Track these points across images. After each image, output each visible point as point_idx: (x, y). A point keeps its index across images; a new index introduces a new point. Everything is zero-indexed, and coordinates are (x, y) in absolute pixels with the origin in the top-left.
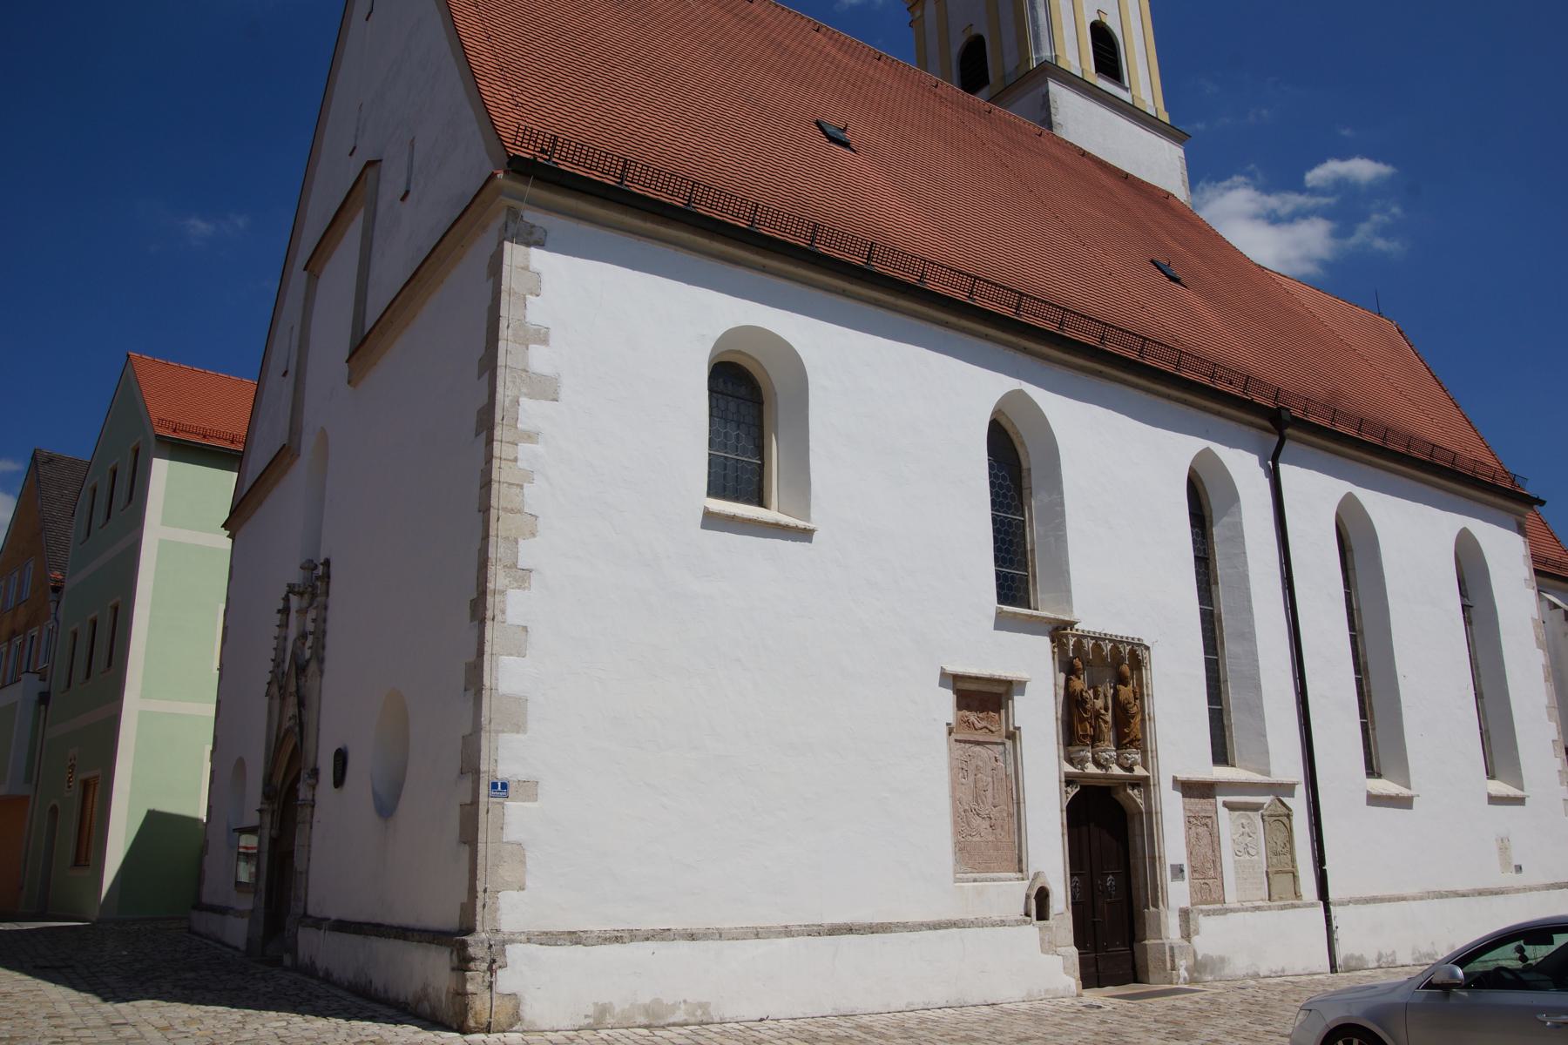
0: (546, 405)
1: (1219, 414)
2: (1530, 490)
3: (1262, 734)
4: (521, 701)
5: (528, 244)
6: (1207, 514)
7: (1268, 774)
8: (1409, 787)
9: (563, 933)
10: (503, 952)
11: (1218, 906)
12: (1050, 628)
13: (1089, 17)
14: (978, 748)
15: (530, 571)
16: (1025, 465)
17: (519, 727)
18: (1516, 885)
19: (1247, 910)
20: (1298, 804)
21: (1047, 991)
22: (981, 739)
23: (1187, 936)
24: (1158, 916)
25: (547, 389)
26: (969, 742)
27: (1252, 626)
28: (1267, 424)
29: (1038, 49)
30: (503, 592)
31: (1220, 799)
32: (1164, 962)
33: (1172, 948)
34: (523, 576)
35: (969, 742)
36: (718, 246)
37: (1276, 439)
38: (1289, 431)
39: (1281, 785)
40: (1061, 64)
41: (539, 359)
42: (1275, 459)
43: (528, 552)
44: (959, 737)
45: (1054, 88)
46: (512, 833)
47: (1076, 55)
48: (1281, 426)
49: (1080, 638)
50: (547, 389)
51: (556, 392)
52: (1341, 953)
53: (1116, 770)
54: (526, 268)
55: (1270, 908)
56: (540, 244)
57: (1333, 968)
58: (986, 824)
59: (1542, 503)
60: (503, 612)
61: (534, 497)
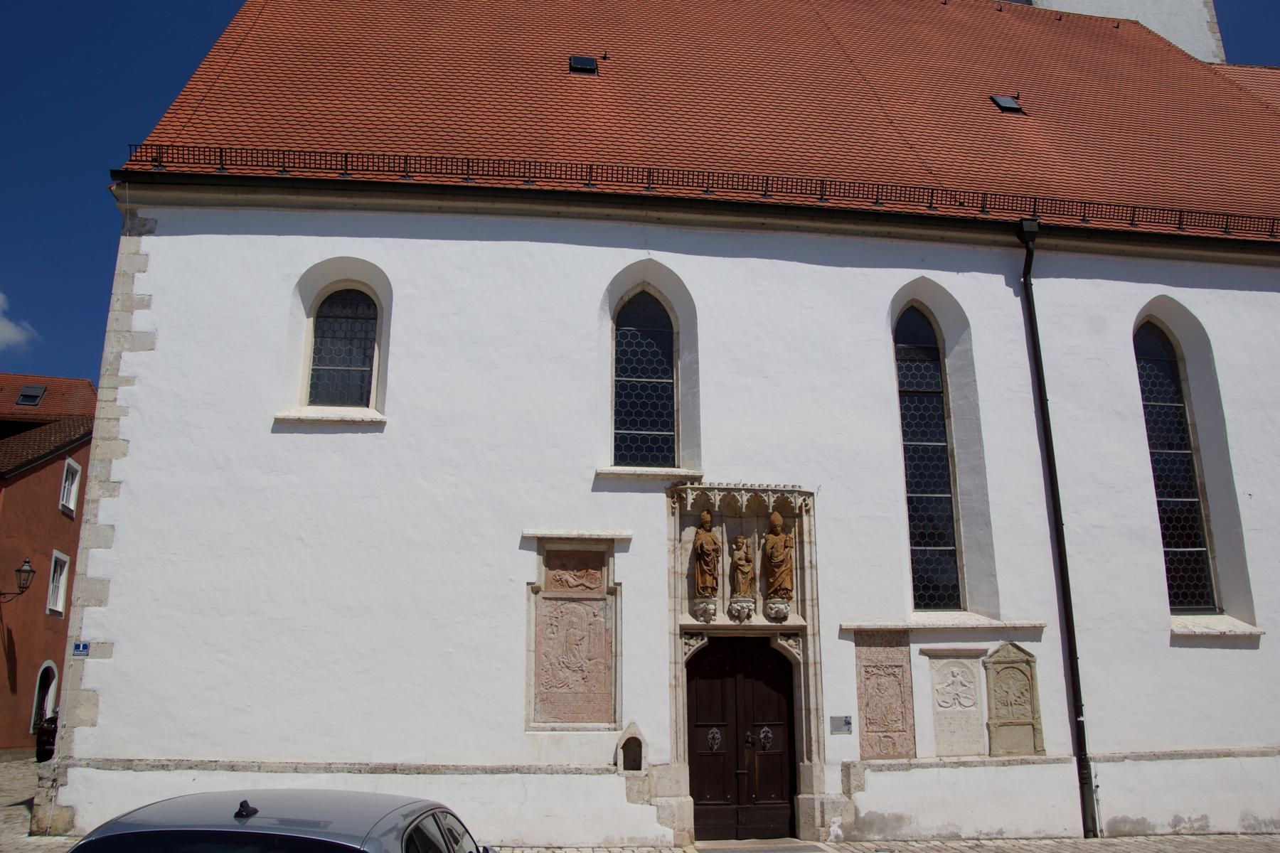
0: (143, 355)
4: (104, 583)
5: (140, 235)
6: (940, 346)
7: (997, 617)
8: (1254, 624)
9: (120, 760)
10: (66, 773)
11: (905, 761)
12: (668, 485)
14: (574, 605)
15: (120, 483)
16: (675, 330)
17: (101, 602)
19: (944, 766)
20: (1048, 653)
21: (631, 839)
22: (575, 596)
23: (847, 792)
24: (816, 771)
25: (146, 342)
26: (562, 599)
27: (982, 458)
28: (1015, 239)
30: (96, 501)
31: (915, 648)
32: (813, 818)
33: (822, 804)
34: (113, 487)
35: (562, 599)
36: (305, 199)
37: (1023, 252)
38: (1038, 241)
39: (1015, 628)
41: (141, 321)
42: (1027, 273)
43: (119, 469)
44: (548, 595)
46: (88, 683)
48: (1027, 238)
49: (704, 492)
50: (146, 342)
51: (153, 343)
52: (1104, 816)
53: (758, 620)
54: (137, 253)
55: (991, 764)
56: (150, 232)
57: (1090, 829)
58: (579, 676)
60: (96, 516)
61: (126, 427)
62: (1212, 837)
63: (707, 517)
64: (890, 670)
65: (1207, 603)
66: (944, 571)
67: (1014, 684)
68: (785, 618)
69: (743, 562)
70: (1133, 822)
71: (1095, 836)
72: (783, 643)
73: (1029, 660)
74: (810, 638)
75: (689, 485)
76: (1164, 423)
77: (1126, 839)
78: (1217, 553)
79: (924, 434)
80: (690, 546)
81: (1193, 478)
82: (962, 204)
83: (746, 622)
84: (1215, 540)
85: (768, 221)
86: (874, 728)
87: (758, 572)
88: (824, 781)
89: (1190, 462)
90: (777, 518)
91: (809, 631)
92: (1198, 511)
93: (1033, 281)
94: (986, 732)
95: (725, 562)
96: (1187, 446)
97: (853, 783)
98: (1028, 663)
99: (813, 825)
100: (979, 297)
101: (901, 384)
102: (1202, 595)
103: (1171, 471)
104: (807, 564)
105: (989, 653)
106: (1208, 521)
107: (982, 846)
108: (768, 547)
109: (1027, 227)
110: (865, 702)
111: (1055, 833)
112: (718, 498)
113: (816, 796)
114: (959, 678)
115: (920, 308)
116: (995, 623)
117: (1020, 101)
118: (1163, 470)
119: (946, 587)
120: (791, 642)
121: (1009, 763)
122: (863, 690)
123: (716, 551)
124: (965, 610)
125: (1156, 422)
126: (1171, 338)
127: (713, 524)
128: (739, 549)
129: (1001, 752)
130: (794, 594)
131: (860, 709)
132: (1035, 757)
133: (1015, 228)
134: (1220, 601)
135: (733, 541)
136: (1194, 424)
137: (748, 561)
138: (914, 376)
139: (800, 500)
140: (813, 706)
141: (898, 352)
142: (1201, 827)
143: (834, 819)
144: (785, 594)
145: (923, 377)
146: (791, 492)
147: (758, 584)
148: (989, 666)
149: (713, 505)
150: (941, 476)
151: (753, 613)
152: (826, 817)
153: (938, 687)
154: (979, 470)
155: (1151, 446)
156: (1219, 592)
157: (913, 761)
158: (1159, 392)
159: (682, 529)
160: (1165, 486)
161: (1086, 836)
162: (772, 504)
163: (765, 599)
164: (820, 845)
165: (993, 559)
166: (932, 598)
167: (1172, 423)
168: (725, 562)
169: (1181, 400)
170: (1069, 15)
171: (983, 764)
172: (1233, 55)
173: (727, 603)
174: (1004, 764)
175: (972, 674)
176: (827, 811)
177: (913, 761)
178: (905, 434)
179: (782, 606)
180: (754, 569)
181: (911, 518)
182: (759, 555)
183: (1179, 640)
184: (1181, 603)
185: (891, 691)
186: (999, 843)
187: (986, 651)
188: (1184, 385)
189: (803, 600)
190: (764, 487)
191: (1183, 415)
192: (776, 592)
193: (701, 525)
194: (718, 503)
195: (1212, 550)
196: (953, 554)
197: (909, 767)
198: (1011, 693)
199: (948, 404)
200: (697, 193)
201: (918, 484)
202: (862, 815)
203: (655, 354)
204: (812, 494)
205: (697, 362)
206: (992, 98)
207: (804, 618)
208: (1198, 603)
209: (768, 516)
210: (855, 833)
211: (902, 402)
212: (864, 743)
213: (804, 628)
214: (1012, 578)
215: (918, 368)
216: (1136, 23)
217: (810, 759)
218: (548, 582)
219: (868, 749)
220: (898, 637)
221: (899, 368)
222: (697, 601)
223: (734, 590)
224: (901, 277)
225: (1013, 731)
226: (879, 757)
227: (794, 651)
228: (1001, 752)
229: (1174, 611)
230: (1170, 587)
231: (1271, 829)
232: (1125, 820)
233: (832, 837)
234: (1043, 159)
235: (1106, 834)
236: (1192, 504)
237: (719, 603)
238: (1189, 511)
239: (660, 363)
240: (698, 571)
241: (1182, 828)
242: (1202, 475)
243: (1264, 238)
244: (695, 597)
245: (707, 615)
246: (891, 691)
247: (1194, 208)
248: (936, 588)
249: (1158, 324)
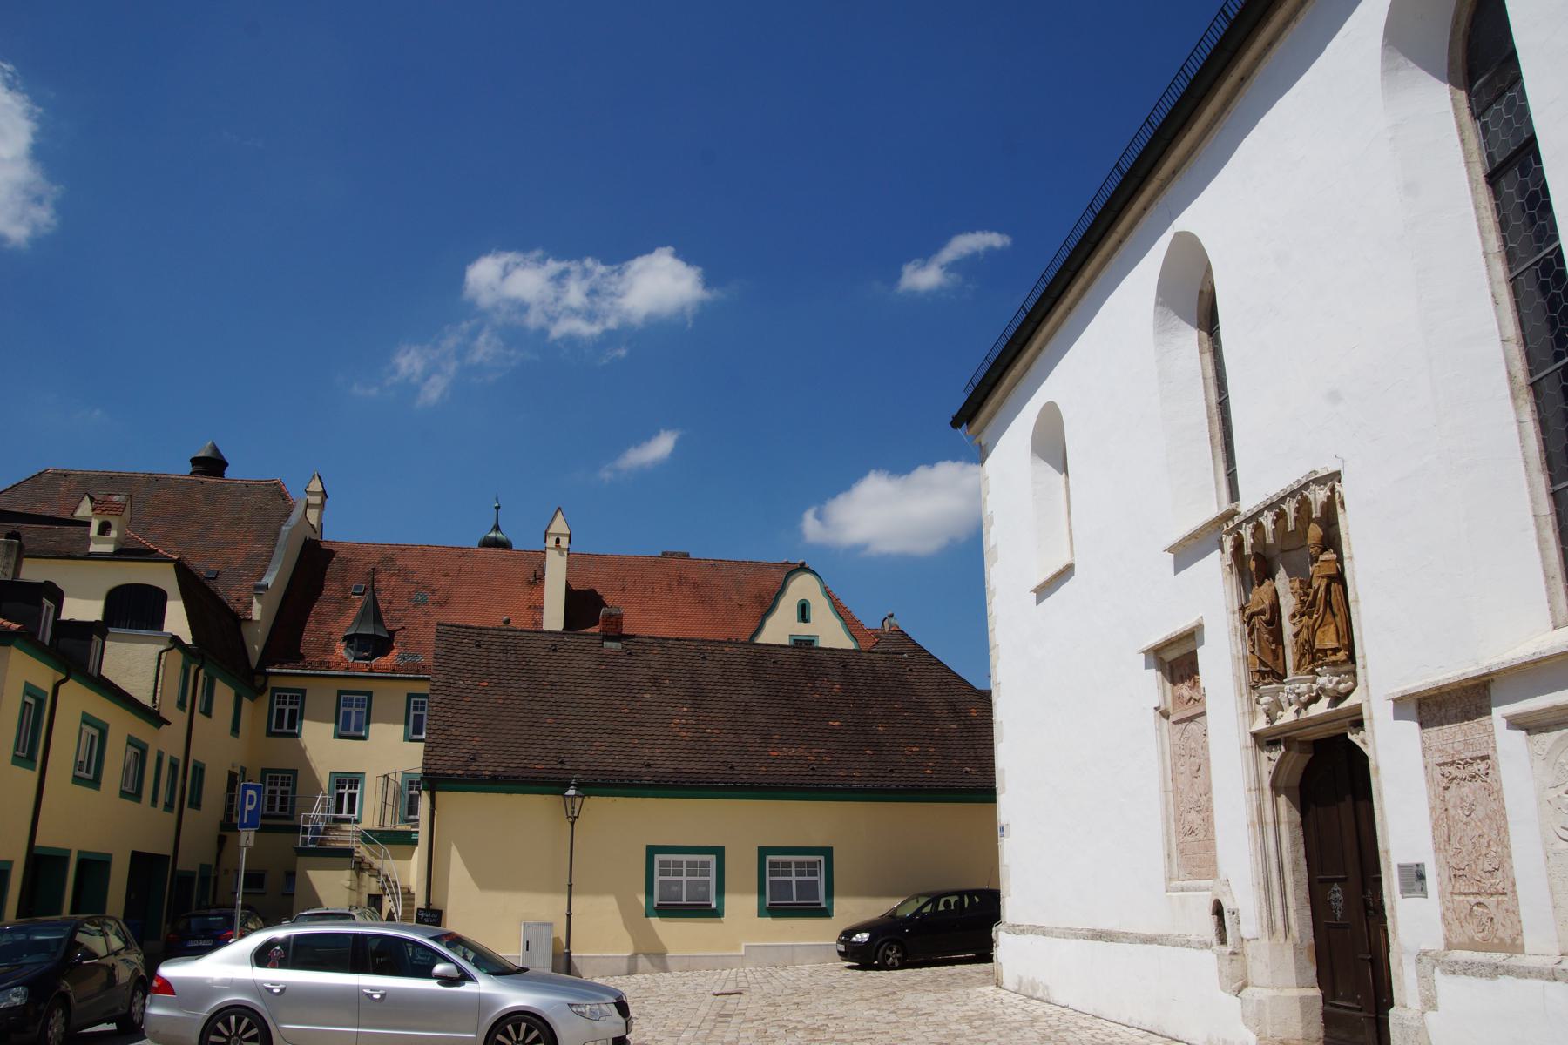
31: (1499, 713)
59: (168, 723)
110: (1445, 839)
157: (1517, 961)
177: (1517, 961)
197: (1495, 971)
218: (1178, 698)
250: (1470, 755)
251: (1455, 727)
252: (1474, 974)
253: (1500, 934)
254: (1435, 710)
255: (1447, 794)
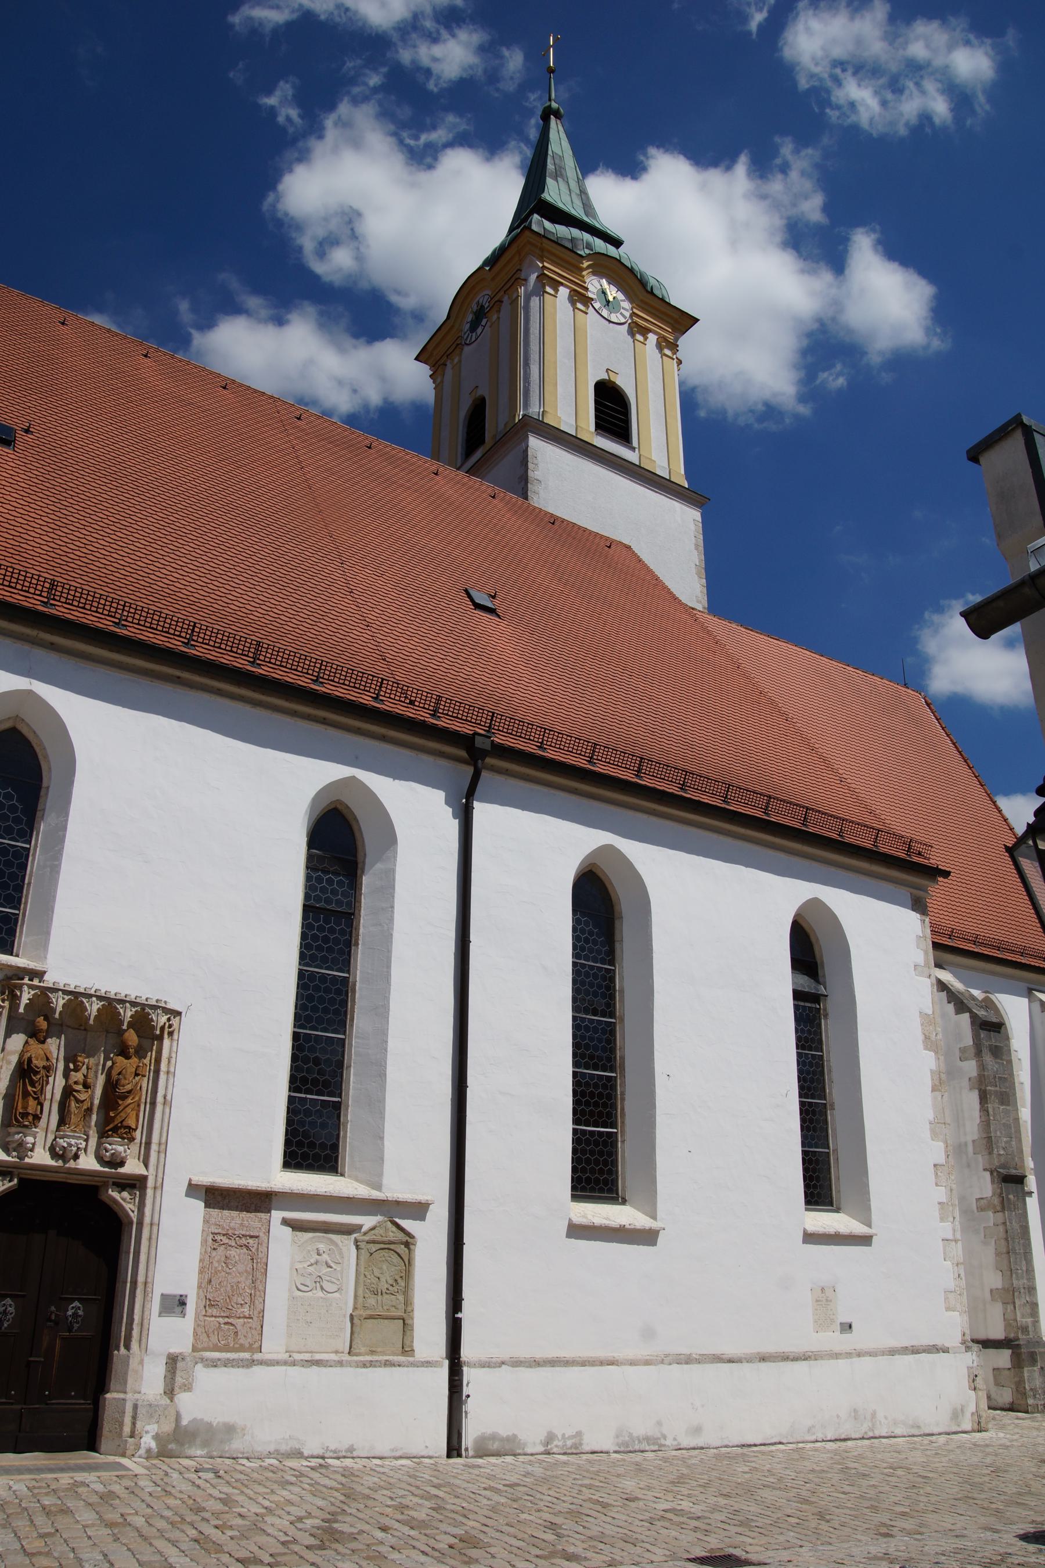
1: (383, 738)
2: (935, 859)
3: (379, 1137)
6: (360, 859)
7: (378, 1187)
11: (246, 1355)
13: (594, 374)
16: (45, 784)
18: (837, 1349)
19: (294, 1364)
20: (431, 1237)
23: (170, 1392)
24: (133, 1363)
27: (386, 999)
28: (463, 754)
29: (526, 405)
31: (277, 1215)
32: (121, 1424)
33: (135, 1407)
37: (470, 770)
39: (398, 1203)
40: (549, 420)
45: (535, 443)
47: (570, 408)
48: (477, 757)
49: (45, 993)
52: (471, 1433)
53: (88, 1162)
55: (349, 1364)
57: (454, 1449)
59: (946, 874)
62: (584, 1457)
63: (43, 1024)
64: (244, 1241)
65: (610, 1191)
66: (324, 1126)
67: (387, 1270)
68: (122, 1164)
69: (80, 1087)
70: (502, 1440)
71: (459, 1455)
72: (115, 1194)
73: (408, 1241)
74: (149, 1192)
75: (26, 981)
76: (591, 985)
77: (493, 1460)
78: (627, 1137)
79: (325, 960)
80: (14, 1059)
81: (613, 1050)
82: (412, 703)
83: (72, 1164)
84: (627, 1121)
85: (186, 675)
86: (215, 1312)
87: (97, 1102)
88: (142, 1376)
89: (613, 1033)
90: (132, 1038)
91: (150, 1183)
92: (614, 1087)
93: (476, 804)
94: (349, 1325)
95: (56, 1085)
96: (612, 1015)
97: (179, 1380)
98: (407, 1245)
99: (120, 1434)
100: (413, 810)
101: (307, 896)
102: (606, 1182)
103: (591, 1039)
104: (160, 1099)
105: (364, 1229)
106: (623, 1099)
107: (326, 1467)
108: (114, 1073)
109: (479, 742)
110: (208, 1278)
111: (414, 1451)
112: (61, 1002)
113: (129, 1396)
114: (325, 1257)
115: (345, 811)
116: (375, 1194)
117: (496, 601)
118: (583, 1038)
119: (323, 1146)
120: (125, 1194)
121: (371, 1364)
122: (207, 1262)
123: (48, 1069)
124: (342, 1175)
125: (583, 983)
126: (612, 895)
127: (49, 1034)
128: (77, 1069)
129: (363, 1350)
130: (138, 1134)
131: (200, 1287)
132: (402, 1359)
133: (466, 742)
134: (624, 1190)
135: (71, 1058)
136: (622, 991)
137: (86, 1086)
138: (323, 890)
139: (163, 1019)
140: (141, 1279)
141: (310, 858)
142: (575, 1446)
143: (148, 1428)
144: (126, 1132)
145: (334, 892)
146: (155, 1007)
147: (94, 1117)
148: (362, 1245)
149: (54, 1010)
150: (337, 1012)
151: (82, 1154)
152: (139, 1424)
153: (299, 1266)
154: (382, 1011)
155: (575, 1009)
156: (624, 1179)
157: (257, 1356)
158: (591, 951)
159: (8, 1035)
160: (583, 1056)
161: (449, 1456)
162: (128, 1019)
163: (100, 1137)
164: (125, 1461)
165: (383, 1118)
166: (305, 1157)
167: (600, 987)
168: (56, 1085)
169: (612, 962)
170: (563, 521)
171: (340, 1363)
172: (714, 608)
173: (51, 1137)
174: (364, 1366)
175: (341, 1254)
176: (140, 1416)
177: (257, 1356)
178: (302, 956)
179: (121, 1149)
180: (92, 1098)
181: (294, 1058)
182: (101, 1080)
183: (577, 1231)
184: (583, 1189)
185: (241, 1267)
186: (348, 1462)
187: (360, 1227)
188: (617, 945)
189: (148, 1144)
190: (122, 997)
191: (612, 980)
192: (115, 1130)
193: (35, 1034)
194: (59, 1009)
195: (623, 1132)
196: (337, 1107)
197: (252, 1363)
198: (383, 1279)
199: (358, 929)
200: (106, 624)
201: (308, 1019)
202: (184, 1422)
203: (13, 809)
204: (179, 1014)
205: (65, 828)
206: (466, 591)
207: (146, 1166)
208: (601, 1190)
209: (121, 1033)
210: (172, 1446)
211: (305, 917)
212: (200, 1330)
213: (144, 1179)
214: (400, 1144)
215: (330, 882)
216: (629, 547)
217: (128, 1347)
219: (204, 1338)
220: (258, 1201)
221: (308, 878)
222: (12, 1130)
223: (62, 1122)
224: (333, 772)
225: (379, 1325)
226: (216, 1349)
227: (128, 1207)
228: (363, 1350)
229: (575, 1198)
230: (574, 1170)
231: (644, 1446)
232: (494, 1437)
233: (142, 1452)
234: (509, 673)
235: (471, 1453)
236: (609, 1078)
237: (41, 1135)
238: (605, 1087)
239: (17, 821)
240: (19, 1092)
241: (555, 1446)
242: (622, 1048)
243: (718, 803)
244: (10, 1125)
245: (22, 1150)
246: (241, 1267)
247: (655, 758)
248: (312, 1145)
249: (600, 875)
250: (244, 1233)
251: (234, 1213)
252: (233, 1366)
253: (241, 1341)
254: (219, 1198)
255: (214, 1253)
